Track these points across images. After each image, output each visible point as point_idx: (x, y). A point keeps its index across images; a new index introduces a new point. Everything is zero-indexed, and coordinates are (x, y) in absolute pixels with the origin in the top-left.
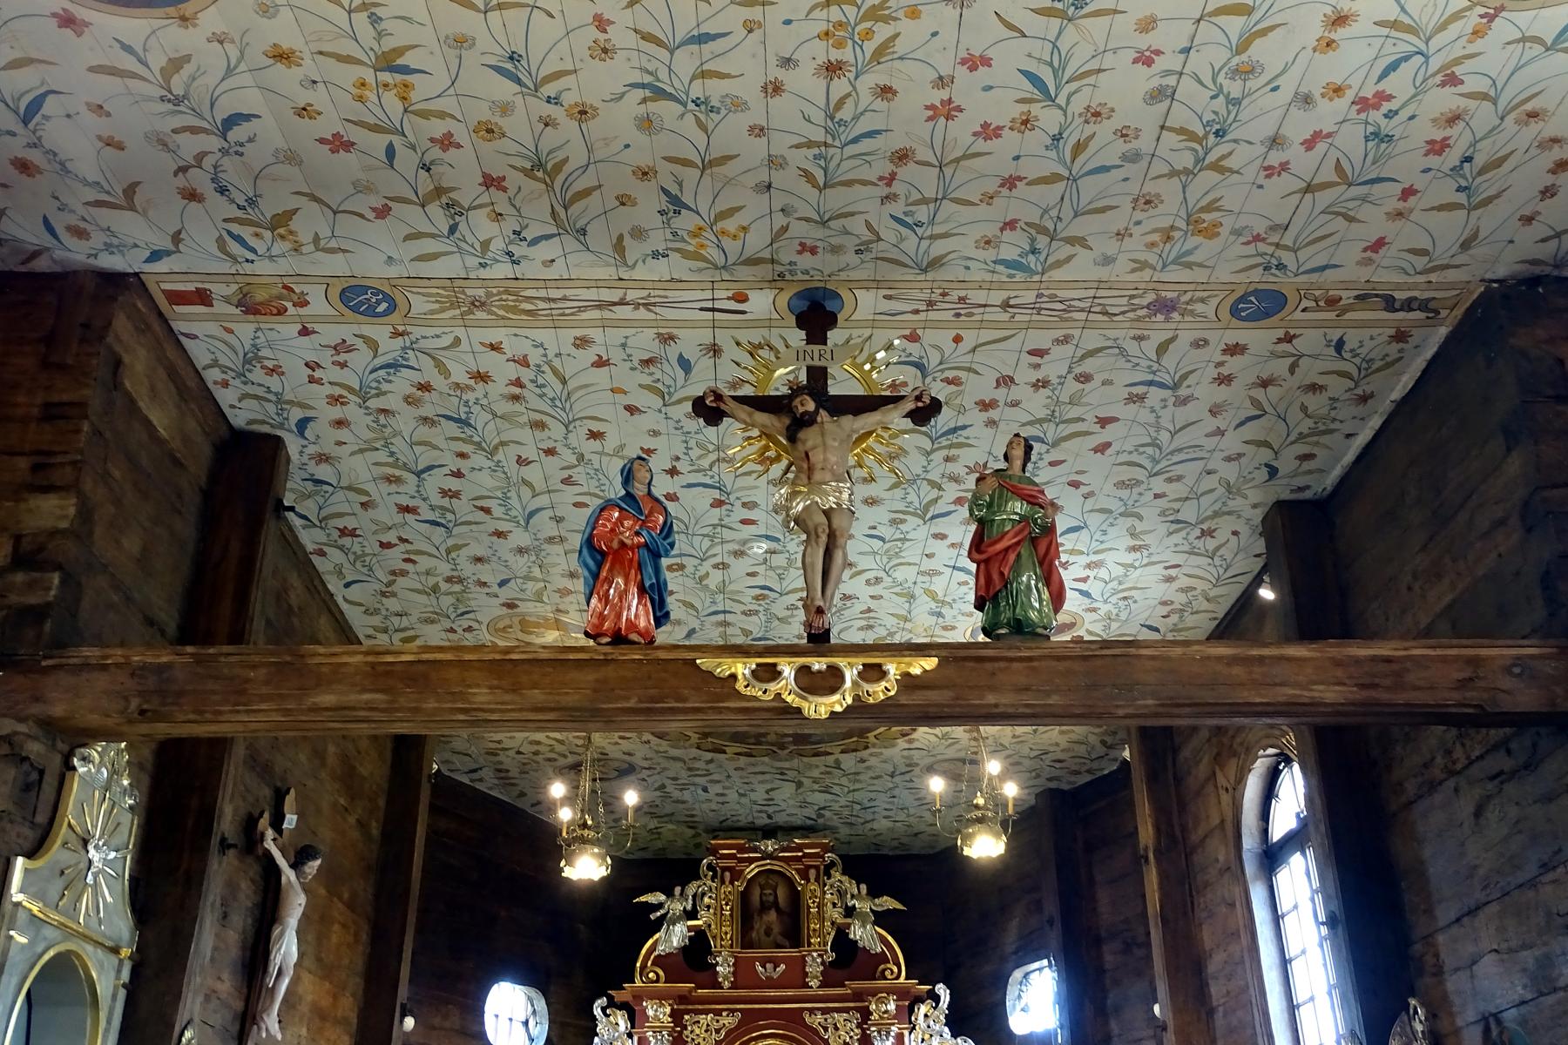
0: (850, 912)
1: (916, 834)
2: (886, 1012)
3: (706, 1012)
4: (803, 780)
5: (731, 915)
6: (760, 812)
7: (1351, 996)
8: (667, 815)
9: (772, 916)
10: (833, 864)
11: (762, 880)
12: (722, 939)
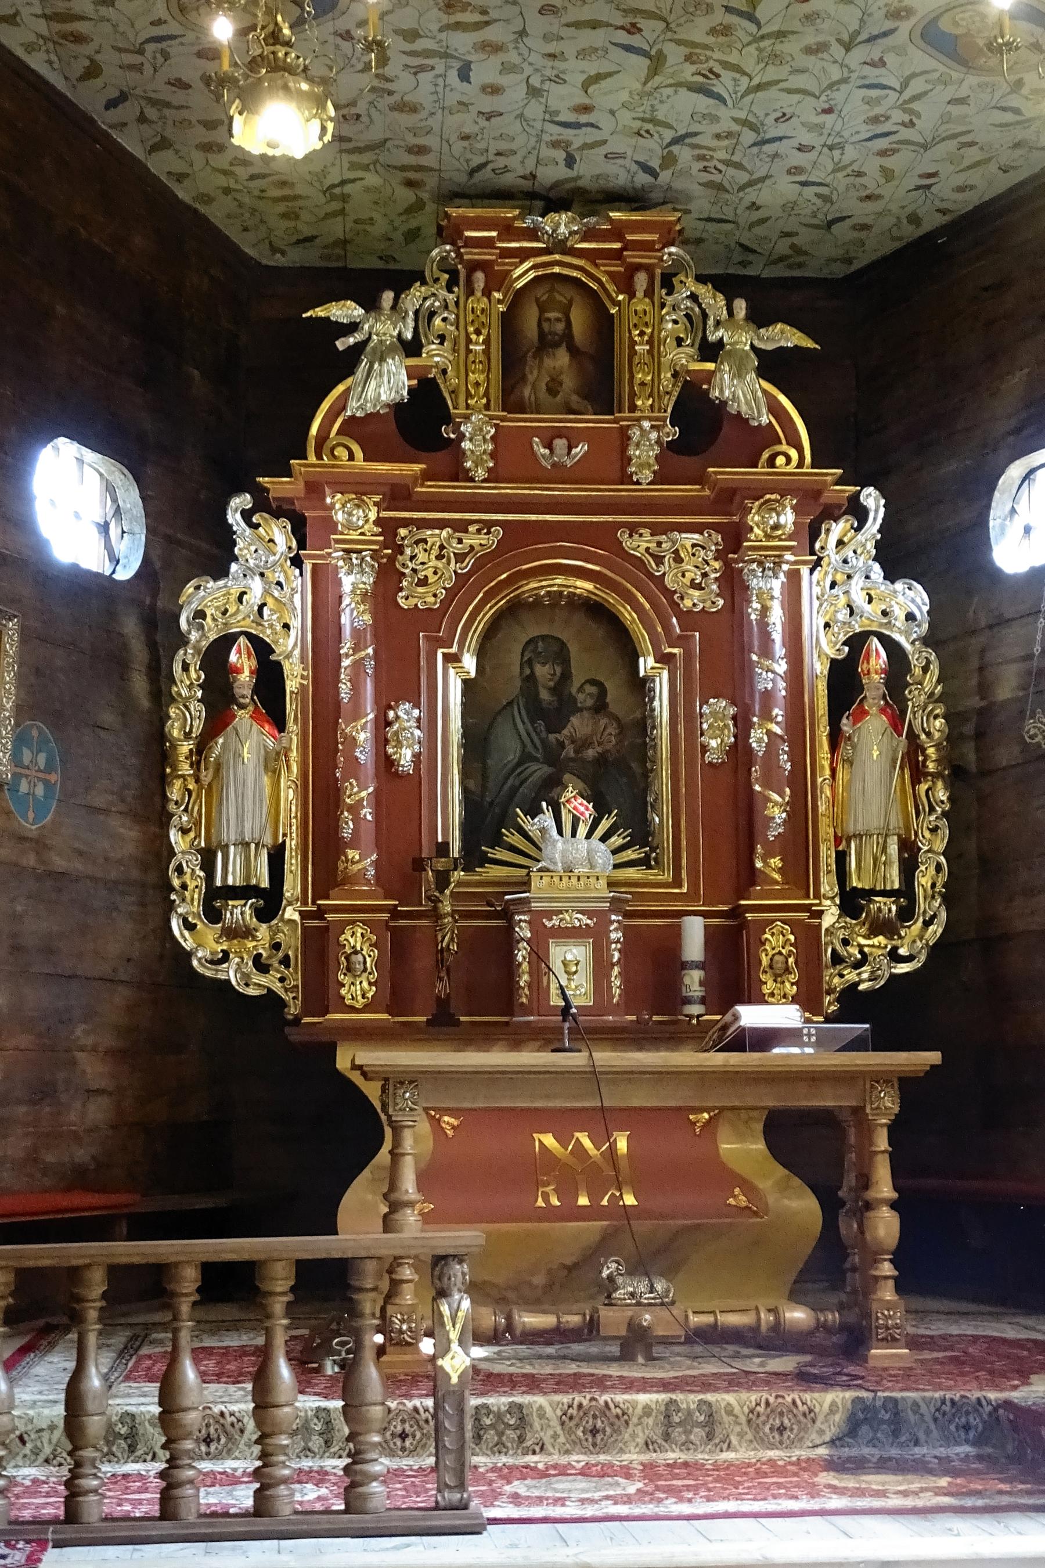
0: (710, 351)
1: (830, 224)
2: (776, 527)
3: (441, 524)
4: (669, 49)
5: (487, 352)
6: (555, 144)
7: (180, 1387)
8: (369, 148)
9: (562, 359)
10: (679, 266)
11: (542, 293)
12: (469, 395)
